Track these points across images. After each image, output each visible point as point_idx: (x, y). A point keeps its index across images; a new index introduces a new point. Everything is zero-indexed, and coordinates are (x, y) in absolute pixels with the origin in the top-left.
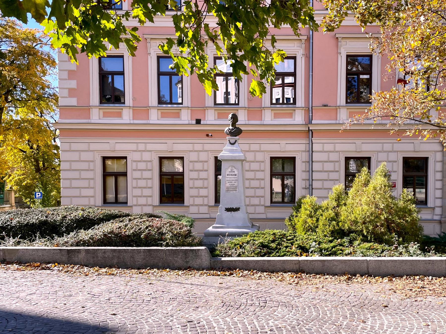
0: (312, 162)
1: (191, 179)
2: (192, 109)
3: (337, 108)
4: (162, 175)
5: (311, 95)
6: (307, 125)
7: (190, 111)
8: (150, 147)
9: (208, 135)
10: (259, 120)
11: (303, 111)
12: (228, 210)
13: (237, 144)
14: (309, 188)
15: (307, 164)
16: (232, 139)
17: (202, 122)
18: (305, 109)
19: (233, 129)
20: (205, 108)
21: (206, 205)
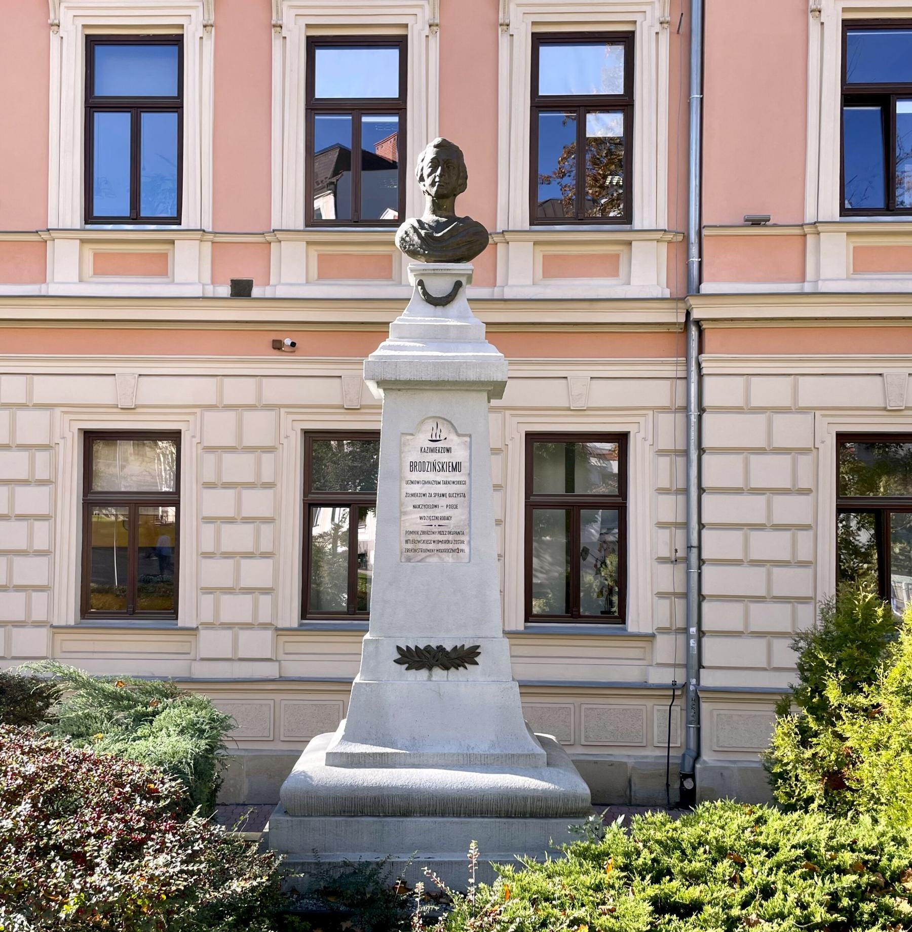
0: (701, 451)
1: (209, 520)
2: (217, 239)
4: (92, 500)
5: (694, 183)
6: (683, 299)
7: (207, 247)
8: (46, 390)
9: (277, 345)
11: (664, 247)
12: (416, 658)
13: (460, 303)
14: (687, 559)
15: (681, 461)
16: (435, 273)
17: (256, 292)
18: (669, 237)
19: (439, 226)
20: (269, 238)
21: (264, 626)
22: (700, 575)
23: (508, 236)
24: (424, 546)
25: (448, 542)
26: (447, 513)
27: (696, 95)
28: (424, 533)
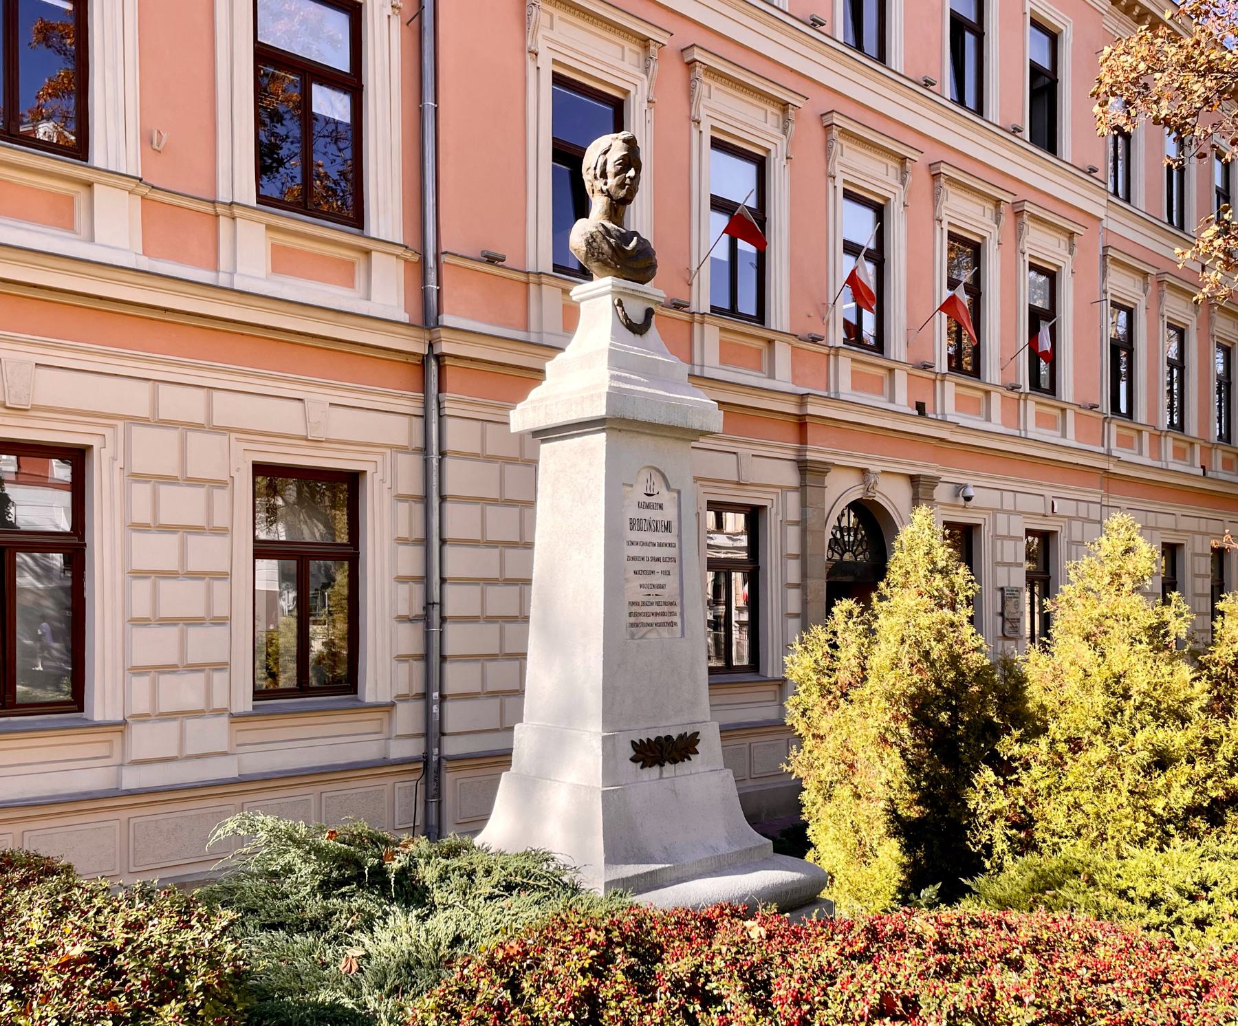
3: (217, 210)
10: (206, 267)
21: (218, 712)
22: (441, 633)
23: (237, 211)
24: (650, 620)
25: (663, 614)
26: (661, 582)
27: (429, 102)
28: (645, 604)
